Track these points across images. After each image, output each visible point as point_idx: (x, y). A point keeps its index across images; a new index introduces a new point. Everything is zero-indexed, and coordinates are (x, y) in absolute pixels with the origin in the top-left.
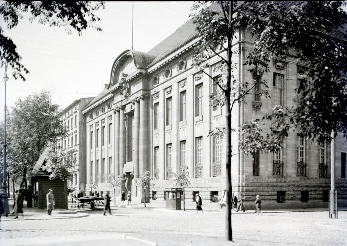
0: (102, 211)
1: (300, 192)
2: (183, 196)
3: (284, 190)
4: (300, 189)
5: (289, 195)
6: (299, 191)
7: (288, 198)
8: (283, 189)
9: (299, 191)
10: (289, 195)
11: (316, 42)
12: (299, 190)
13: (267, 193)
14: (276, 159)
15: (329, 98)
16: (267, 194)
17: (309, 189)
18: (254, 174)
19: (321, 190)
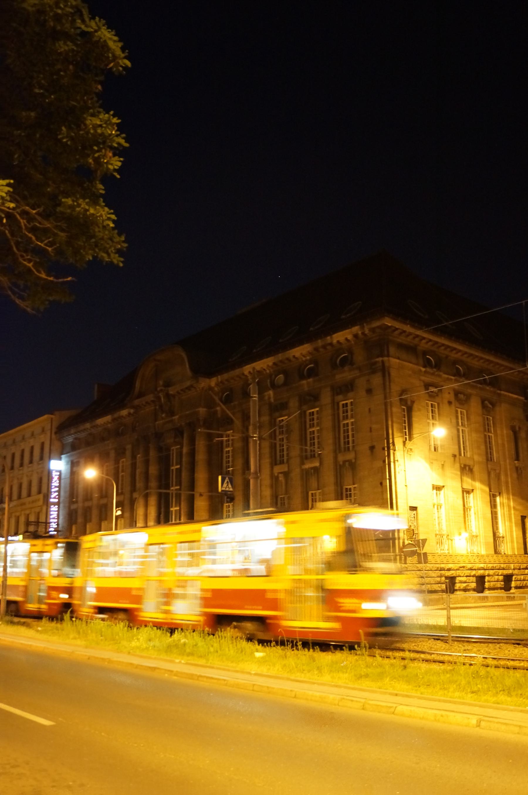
0: (387, 364)
1: (474, 579)
2: (401, 707)
3: (454, 575)
4: (474, 573)
5: (461, 582)
6: (473, 576)
7: (460, 587)
8: (452, 574)
9: (473, 576)
10: (461, 582)
11: (58, 466)
12: (472, 574)
13: (432, 580)
14: (18, 563)
15: (74, 279)
16: (432, 582)
17: (487, 572)
18: (410, 507)
19: (500, 574)
